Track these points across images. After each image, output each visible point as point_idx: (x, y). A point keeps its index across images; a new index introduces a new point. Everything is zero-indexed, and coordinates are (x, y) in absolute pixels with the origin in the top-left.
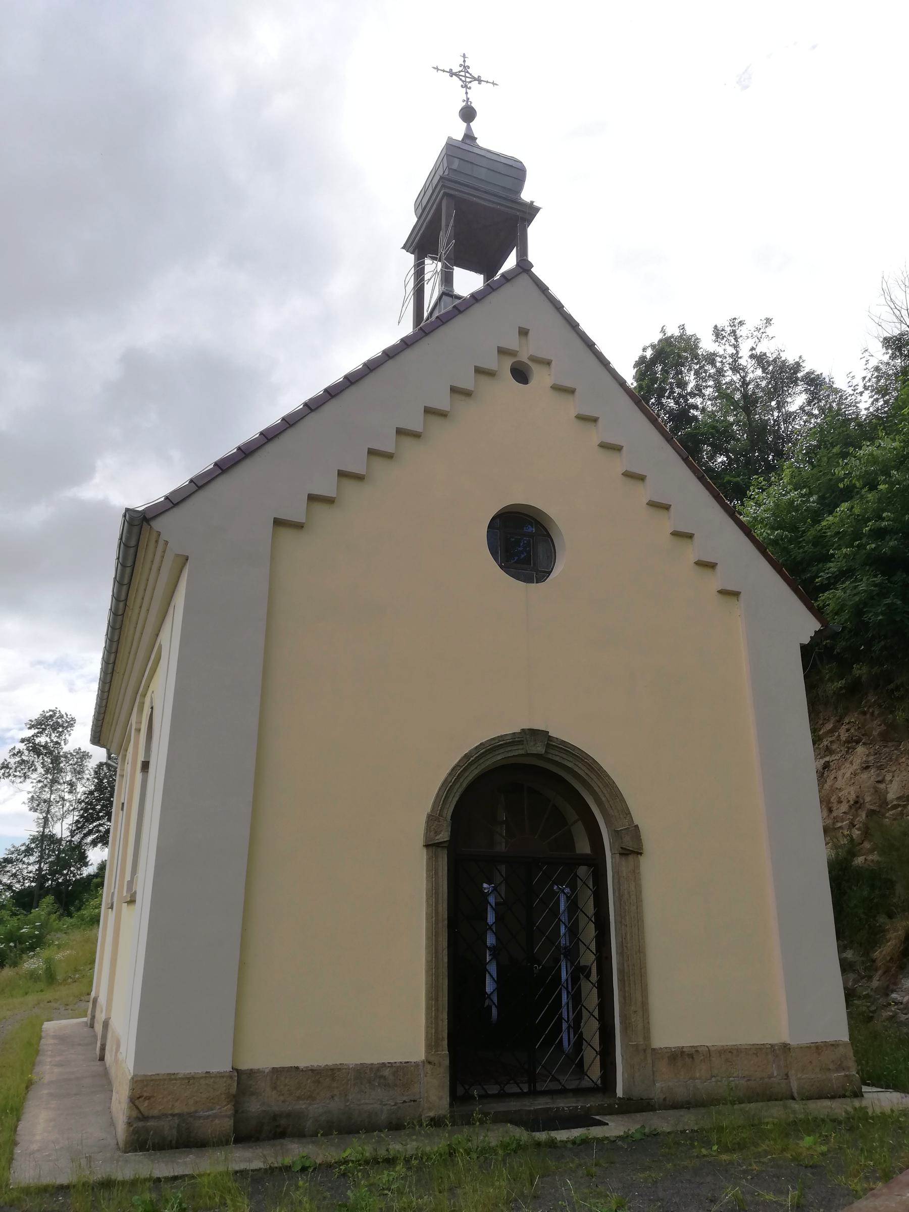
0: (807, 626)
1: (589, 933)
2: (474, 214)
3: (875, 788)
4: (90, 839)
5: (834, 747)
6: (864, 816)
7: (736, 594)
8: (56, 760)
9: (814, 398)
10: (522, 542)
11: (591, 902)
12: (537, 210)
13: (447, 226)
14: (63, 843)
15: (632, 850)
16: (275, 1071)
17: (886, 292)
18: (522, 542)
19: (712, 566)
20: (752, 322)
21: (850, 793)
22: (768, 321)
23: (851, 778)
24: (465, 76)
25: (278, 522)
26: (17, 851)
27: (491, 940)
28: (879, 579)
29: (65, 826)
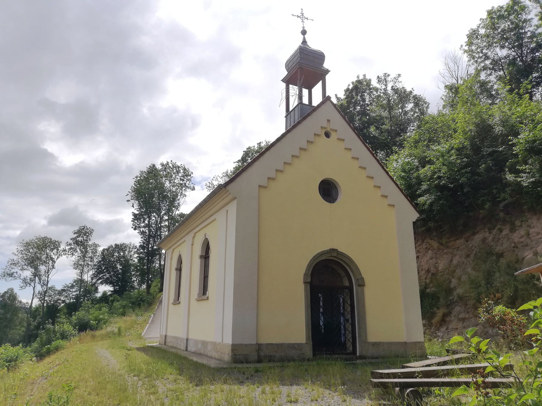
0: (415, 215)
1: (349, 309)
2: (306, 68)
5: (421, 250)
7: (393, 206)
8: (85, 248)
9: (417, 105)
10: (328, 190)
11: (349, 300)
12: (329, 71)
13: (301, 79)
15: (362, 284)
17: (446, 64)
18: (328, 190)
19: (386, 197)
20: (393, 75)
21: (426, 267)
22: (399, 75)
24: (302, 17)
25: (260, 186)
27: (321, 310)
28: (439, 194)
29: (89, 276)
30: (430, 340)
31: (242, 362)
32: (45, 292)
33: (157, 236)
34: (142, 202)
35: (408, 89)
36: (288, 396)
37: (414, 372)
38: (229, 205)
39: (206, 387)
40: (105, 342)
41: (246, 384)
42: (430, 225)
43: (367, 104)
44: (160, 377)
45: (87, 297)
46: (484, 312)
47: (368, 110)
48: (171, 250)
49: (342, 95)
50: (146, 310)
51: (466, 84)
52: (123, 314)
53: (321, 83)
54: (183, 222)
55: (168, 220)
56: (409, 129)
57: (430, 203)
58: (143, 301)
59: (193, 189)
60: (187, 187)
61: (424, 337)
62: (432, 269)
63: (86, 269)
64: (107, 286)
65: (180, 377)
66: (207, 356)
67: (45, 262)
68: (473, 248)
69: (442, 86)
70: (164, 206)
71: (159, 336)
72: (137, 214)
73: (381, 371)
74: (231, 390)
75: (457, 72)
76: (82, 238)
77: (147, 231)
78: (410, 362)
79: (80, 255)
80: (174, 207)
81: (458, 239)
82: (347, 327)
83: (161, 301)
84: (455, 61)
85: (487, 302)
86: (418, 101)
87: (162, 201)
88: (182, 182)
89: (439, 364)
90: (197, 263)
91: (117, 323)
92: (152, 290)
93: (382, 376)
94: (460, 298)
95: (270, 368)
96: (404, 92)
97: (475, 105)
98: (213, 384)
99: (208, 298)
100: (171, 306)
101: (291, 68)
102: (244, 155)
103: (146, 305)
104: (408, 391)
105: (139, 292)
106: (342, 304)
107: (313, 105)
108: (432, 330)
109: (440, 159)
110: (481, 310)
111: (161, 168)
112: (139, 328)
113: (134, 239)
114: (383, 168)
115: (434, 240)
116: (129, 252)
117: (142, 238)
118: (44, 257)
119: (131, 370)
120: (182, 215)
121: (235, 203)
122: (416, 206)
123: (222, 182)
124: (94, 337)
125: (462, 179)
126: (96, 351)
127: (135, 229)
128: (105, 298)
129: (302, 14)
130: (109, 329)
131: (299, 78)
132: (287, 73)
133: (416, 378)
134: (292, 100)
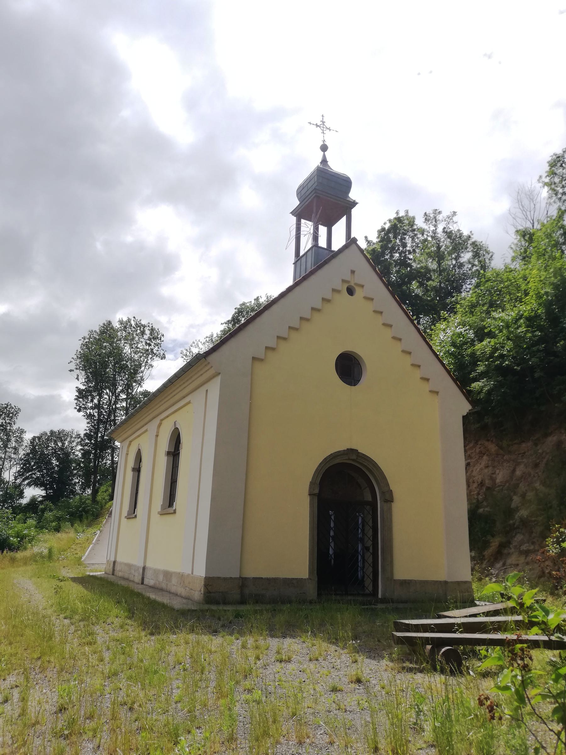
0: (465, 407)
1: (370, 533)
2: (326, 197)
3: (491, 477)
6: (484, 489)
7: (437, 393)
8: (8, 435)
9: (476, 255)
10: (349, 368)
11: (371, 521)
12: (357, 203)
13: (317, 212)
14: (10, 483)
15: (389, 498)
18: (349, 368)
19: (428, 380)
20: (446, 213)
21: (478, 478)
23: (481, 470)
24: (322, 126)
25: (254, 358)
27: (332, 533)
28: (500, 378)
29: (11, 474)
30: (480, 580)
31: (218, 603)
33: (110, 421)
34: (90, 373)
35: (466, 233)
36: (278, 652)
37: (453, 624)
38: (194, 393)
39: (165, 637)
40: (29, 568)
41: (221, 635)
42: (486, 421)
43: (409, 251)
44: (101, 621)
45: (7, 503)
46: (553, 543)
47: (410, 259)
48: (127, 442)
49: (374, 238)
50: (89, 525)
51: (544, 229)
53: (344, 219)
54: (146, 404)
55: (126, 400)
56: (464, 287)
57: (488, 390)
58: (87, 512)
59: (163, 357)
61: (472, 575)
62: (487, 481)
64: (37, 489)
65: (129, 621)
66: (170, 592)
68: (544, 454)
69: (512, 231)
70: (122, 380)
71: (105, 562)
72: (83, 390)
73: (407, 622)
74: (198, 643)
75: (532, 213)
77: (96, 414)
78: (448, 609)
80: (135, 381)
81: (524, 442)
82: (366, 558)
83: (111, 513)
84: (531, 196)
85: (559, 531)
86: (478, 250)
87: (120, 373)
88: (147, 347)
89: (487, 614)
90: (163, 461)
91: (46, 542)
92: (99, 498)
93: (409, 628)
94: (524, 523)
95: (256, 612)
96: (460, 237)
97: (554, 259)
98: (174, 633)
99: (175, 512)
100: (124, 520)
101: (304, 197)
103: (90, 518)
104: (443, 650)
105: (81, 499)
106: (361, 526)
107: (333, 249)
108: (484, 566)
109: (504, 332)
110: (550, 540)
111: (119, 326)
112: (79, 549)
113: (79, 425)
114: (425, 339)
115: (492, 441)
116: (70, 442)
117: (88, 423)
119: (61, 610)
120: (146, 394)
121: (217, 381)
122: (468, 395)
123: (203, 349)
124: (13, 560)
125: (533, 359)
126: (15, 581)
127: (79, 411)
128: (33, 504)
129: (323, 122)
130: (36, 550)
131: (314, 210)
132: (299, 203)
133: (454, 632)
134: (303, 240)
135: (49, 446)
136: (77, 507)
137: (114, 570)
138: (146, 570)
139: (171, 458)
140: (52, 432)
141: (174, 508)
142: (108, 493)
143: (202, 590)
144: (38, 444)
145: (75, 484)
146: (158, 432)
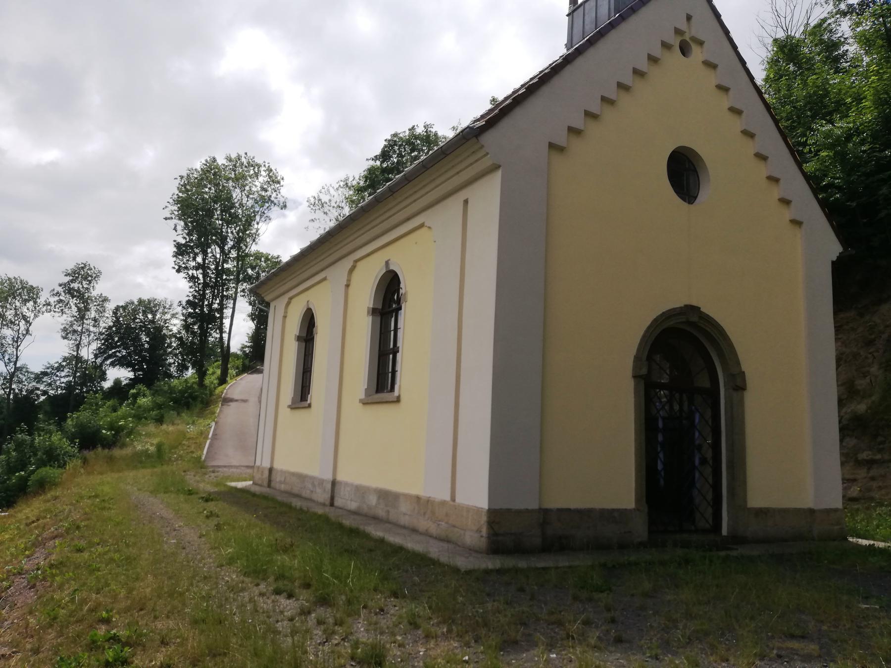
4: (108, 362)
10: (684, 172)
15: (738, 384)
16: (561, 511)
18: (684, 172)
26: (52, 367)
29: (91, 351)
32: (12, 375)
45: (86, 386)
50: (201, 414)
52: (160, 420)
60: (272, 202)
63: (85, 340)
67: (11, 322)
76: (79, 284)
79: (76, 314)
91: (149, 438)
92: (207, 381)
99: (309, 406)
100: (284, 410)
102: (385, 146)
103: (199, 406)
116: (164, 313)
117: (191, 287)
118: (10, 314)
121: (495, 182)
127: (178, 271)
128: (119, 391)
135: (136, 318)
136: (182, 392)
137: (270, 481)
138: (337, 487)
139: (378, 319)
140: (141, 301)
141: (396, 393)
142: (215, 376)
143: (484, 531)
144: (127, 312)
145: (170, 364)
146: (349, 280)
